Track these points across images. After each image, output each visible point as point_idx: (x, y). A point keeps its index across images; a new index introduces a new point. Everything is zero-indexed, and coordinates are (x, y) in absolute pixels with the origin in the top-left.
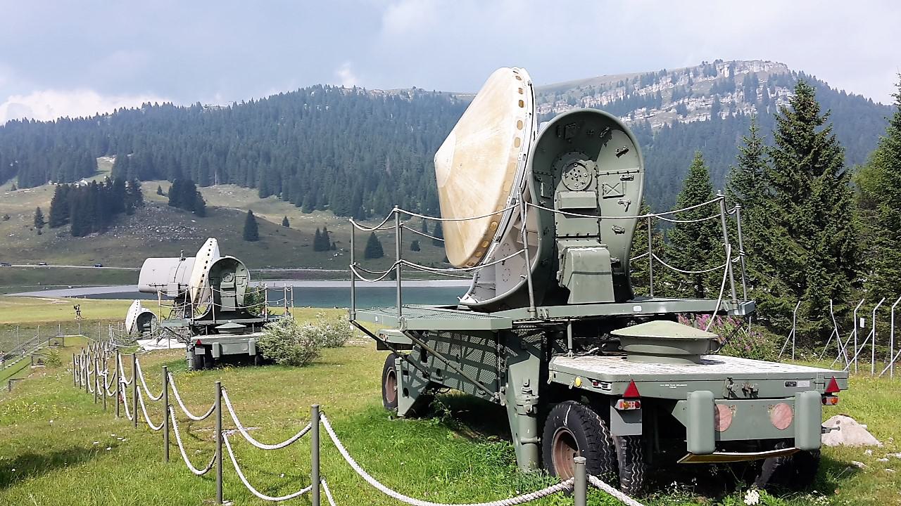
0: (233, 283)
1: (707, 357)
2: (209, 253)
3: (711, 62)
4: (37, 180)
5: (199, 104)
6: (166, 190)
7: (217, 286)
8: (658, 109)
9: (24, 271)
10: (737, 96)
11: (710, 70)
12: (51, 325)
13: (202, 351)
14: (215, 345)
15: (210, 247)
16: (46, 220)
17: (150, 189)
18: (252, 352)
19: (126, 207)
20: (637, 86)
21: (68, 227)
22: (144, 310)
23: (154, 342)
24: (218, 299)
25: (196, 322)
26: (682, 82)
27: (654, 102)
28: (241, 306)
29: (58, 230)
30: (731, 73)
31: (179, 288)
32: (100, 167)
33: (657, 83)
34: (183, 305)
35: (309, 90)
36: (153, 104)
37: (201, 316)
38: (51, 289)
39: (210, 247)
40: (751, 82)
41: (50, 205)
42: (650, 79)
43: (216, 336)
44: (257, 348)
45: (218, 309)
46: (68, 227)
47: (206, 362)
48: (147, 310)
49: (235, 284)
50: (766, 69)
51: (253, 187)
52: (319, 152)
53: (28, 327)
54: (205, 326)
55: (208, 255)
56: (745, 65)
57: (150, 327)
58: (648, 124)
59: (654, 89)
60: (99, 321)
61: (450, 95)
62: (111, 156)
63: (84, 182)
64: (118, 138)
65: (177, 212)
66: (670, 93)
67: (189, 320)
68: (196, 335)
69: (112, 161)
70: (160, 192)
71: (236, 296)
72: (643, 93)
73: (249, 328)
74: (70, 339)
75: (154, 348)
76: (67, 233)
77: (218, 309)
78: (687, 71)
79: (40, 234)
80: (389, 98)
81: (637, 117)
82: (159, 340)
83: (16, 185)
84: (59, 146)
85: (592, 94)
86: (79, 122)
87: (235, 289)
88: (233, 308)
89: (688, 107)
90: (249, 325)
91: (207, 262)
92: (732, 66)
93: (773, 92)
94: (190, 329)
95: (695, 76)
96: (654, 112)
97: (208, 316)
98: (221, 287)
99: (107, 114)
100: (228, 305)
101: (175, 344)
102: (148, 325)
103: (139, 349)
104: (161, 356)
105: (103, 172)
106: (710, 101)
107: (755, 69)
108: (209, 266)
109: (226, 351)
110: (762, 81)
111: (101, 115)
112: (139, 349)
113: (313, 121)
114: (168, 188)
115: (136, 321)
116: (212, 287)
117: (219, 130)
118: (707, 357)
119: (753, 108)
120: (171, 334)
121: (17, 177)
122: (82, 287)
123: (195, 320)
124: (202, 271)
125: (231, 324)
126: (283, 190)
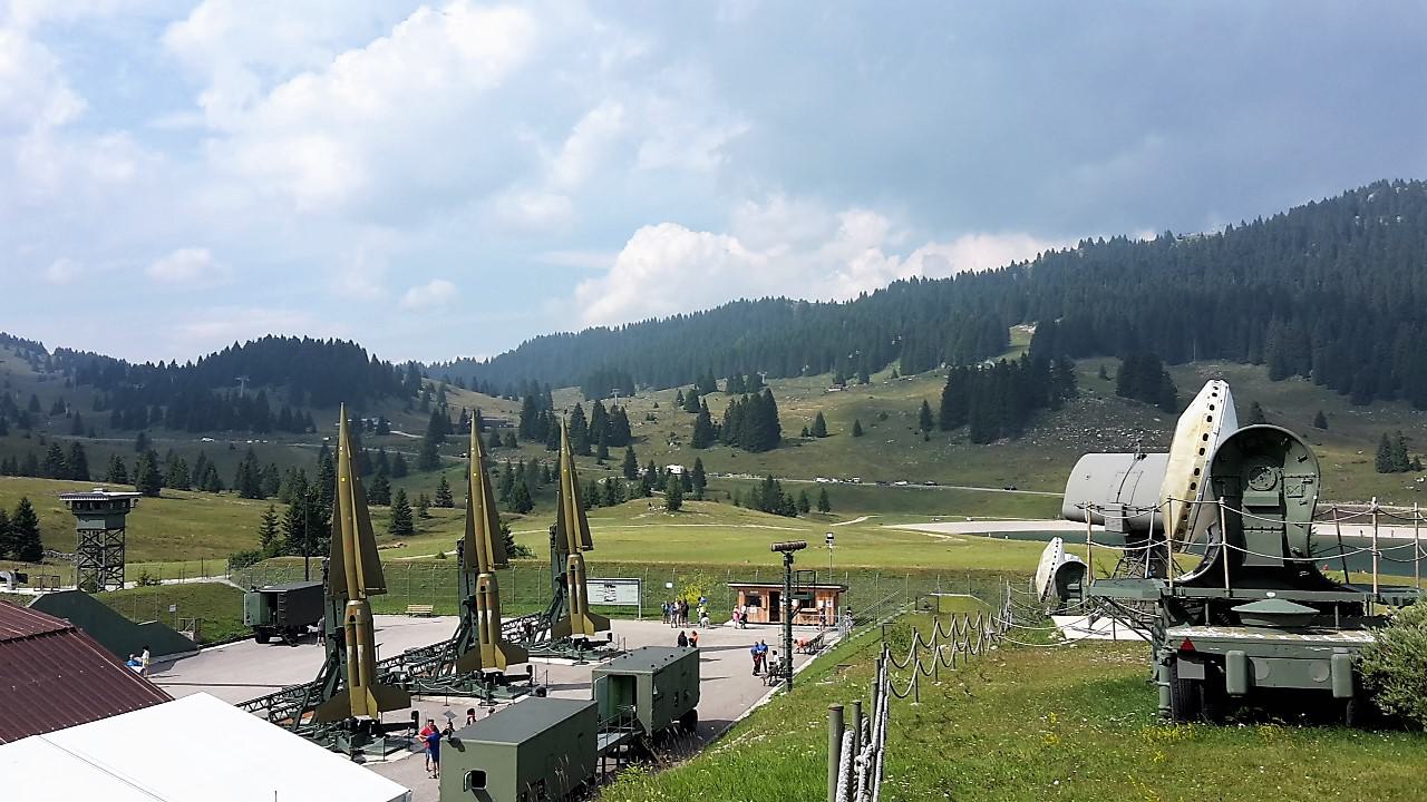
0: (1275, 494)
2: (1207, 418)
4: (921, 364)
5: (1169, 233)
6: (1112, 373)
7: (1235, 499)
9: (871, 490)
12: (926, 575)
13: (1193, 671)
14: (1233, 656)
15: (1213, 401)
16: (936, 419)
17: (1087, 369)
18: (1340, 688)
19: (1051, 399)
21: (967, 430)
22: (1068, 558)
23: (1083, 621)
24: (1236, 533)
25: (1179, 590)
28: (1300, 555)
29: (953, 433)
31: (1124, 514)
32: (1015, 341)
34: (1146, 544)
35: (1364, 192)
36: (1095, 241)
37: (1189, 576)
38: (942, 520)
39: (1213, 401)
41: (941, 397)
43: (1235, 633)
44: (1356, 678)
45: (1236, 558)
46: (967, 430)
47: (1206, 700)
48: (1076, 559)
49: (1281, 497)
51: (1258, 362)
52: (1384, 298)
53: (894, 576)
54: (1202, 602)
55: (1210, 419)
57: (1080, 591)
60: (1000, 573)
62: (1030, 325)
63: (990, 362)
64: (1042, 295)
65: (1130, 404)
67: (1159, 584)
68: (1179, 623)
69: (1032, 330)
70: (1103, 375)
71: (1284, 529)
73: (1325, 617)
74: (953, 601)
75: (1081, 635)
76: (963, 438)
77: (1236, 558)
79: (927, 439)
82: (1093, 620)
83: (898, 370)
84: (958, 311)
86: (988, 275)
87: (1281, 509)
88: (1275, 558)
90: (1326, 608)
91: (1205, 437)
94: (1161, 605)
97: (1211, 577)
98: (1244, 503)
99: (1027, 261)
100: (1263, 550)
101: (1125, 633)
103: (1054, 635)
104: (1096, 658)
105: (1015, 348)
108: (1211, 448)
109: (1265, 676)
111: (1018, 263)
112: (1054, 635)
113: (1372, 243)
114: (1116, 368)
115: (1053, 576)
116: (1221, 501)
117: (1201, 272)
120: (1117, 611)
121: (899, 360)
122: (986, 520)
123: (1176, 584)
124: (1193, 461)
125: (1273, 601)
126: (1314, 364)
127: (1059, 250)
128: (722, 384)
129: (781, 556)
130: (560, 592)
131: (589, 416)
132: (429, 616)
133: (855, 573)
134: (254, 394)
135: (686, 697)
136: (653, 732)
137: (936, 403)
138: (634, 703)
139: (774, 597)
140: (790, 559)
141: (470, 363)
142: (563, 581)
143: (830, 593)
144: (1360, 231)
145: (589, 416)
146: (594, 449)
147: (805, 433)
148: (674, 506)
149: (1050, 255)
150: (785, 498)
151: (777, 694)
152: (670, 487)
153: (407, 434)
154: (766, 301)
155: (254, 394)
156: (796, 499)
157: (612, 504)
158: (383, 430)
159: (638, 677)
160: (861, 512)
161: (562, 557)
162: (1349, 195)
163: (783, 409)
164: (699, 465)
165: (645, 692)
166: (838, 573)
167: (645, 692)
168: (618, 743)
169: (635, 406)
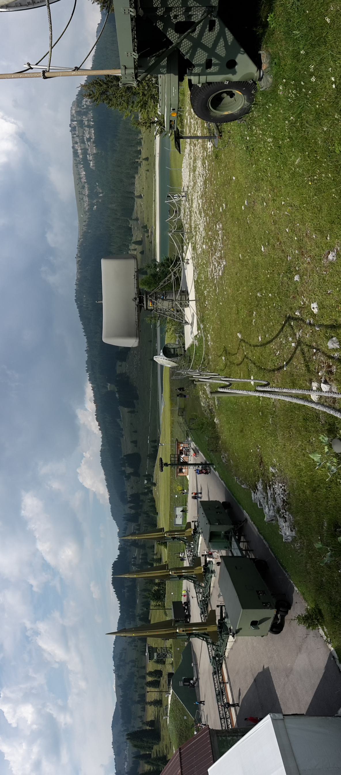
1: (95, 48)
3: (70, 128)
5: (86, 351)
8: (88, 150)
10: (85, 119)
11: (73, 129)
20: (78, 159)
21: (135, 401)
22: (161, 354)
26: (77, 140)
27: (85, 152)
30: (75, 121)
33: (77, 150)
40: (79, 113)
42: (75, 153)
50: (74, 108)
56: (72, 116)
57: (174, 349)
58: (94, 154)
59: (79, 151)
61: (79, 241)
66: (82, 145)
69: (109, 384)
70: (121, 366)
72: (81, 156)
78: (73, 137)
80: (80, 269)
81: (91, 159)
82: (187, 323)
85: (80, 178)
89: (88, 137)
92: (72, 120)
93: (84, 106)
95: (75, 134)
96: (89, 152)
102: (172, 351)
106: (86, 129)
107: (74, 112)
110: (78, 109)
118: (95, 48)
119: (90, 112)
127: (88, 378)
128: (123, 468)
129: (164, 468)
130: (177, 539)
131: (132, 505)
133: (172, 436)
134: (127, 589)
135: (218, 508)
137: (126, 410)
140: (166, 465)
142: (174, 538)
144: (87, 305)
145: (132, 505)
146: (141, 504)
147: (136, 446)
148: (155, 484)
149: (90, 380)
150: (133, 511)
151: (214, 469)
152: (150, 485)
154: (101, 456)
155: (127, 589)
156: (153, 449)
157: (154, 501)
158: (135, 558)
162: (78, 308)
163: (130, 452)
165: (217, 528)
166: (172, 441)
167: (217, 528)
168: (235, 538)
169: (129, 492)
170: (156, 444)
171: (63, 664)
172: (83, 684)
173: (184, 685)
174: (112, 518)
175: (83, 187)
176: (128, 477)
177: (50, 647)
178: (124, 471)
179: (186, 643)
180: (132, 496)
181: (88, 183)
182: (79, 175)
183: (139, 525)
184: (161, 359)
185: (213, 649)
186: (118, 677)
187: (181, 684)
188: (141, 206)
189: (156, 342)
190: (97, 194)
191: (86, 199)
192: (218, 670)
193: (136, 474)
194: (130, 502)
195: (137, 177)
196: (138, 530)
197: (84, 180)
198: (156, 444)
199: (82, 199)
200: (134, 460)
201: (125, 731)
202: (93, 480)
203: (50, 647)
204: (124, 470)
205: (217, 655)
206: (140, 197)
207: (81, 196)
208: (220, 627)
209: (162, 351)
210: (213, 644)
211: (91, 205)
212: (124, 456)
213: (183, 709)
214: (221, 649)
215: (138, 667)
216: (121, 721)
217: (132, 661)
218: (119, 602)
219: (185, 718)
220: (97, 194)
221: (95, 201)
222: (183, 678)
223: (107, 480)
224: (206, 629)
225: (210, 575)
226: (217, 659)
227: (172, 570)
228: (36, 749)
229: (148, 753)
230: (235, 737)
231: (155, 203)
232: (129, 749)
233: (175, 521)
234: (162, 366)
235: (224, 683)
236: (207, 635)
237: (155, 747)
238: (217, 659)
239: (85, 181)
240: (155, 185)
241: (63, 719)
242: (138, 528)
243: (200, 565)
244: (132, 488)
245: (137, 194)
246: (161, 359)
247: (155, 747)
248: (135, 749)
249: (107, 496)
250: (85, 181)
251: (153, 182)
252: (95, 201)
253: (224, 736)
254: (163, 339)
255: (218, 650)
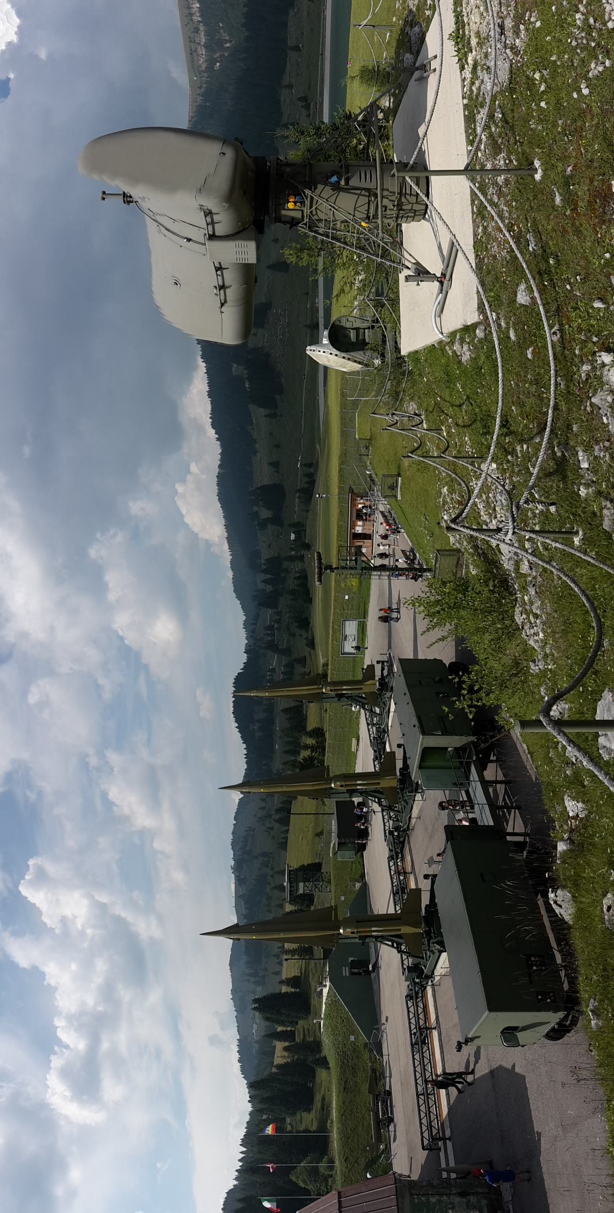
21: (277, 397)
22: (325, 341)
46: (277, 397)
70: (255, 334)
85: (191, 15)
115: (343, 355)
127: (201, 353)
128: (255, 509)
130: (348, 698)
132: (358, 741)
136: (474, 736)
137: (262, 411)
138: (447, 748)
139: (357, 536)
141: (246, 624)
143: (353, 500)
146: (283, 575)
147: (277, 472)
150: (269, 588)
153: (275, 661)
154: (218, 485)
156: (307, 480)
158: (273, 670)
159: (425, 745)
160: (315, 447)
161: (324, 696)
163: (266, 482)
164: (291, 525)
165: (436, 741)
167: (436, 741)
169: (266, 554)
170: (312, 470)
171: (145, 835)
172: (178, 876)
173: (352, 974)
174: (234, 595)
175: (197, 30)
176: (263, 524)
177: (127, 798)
178: (256, 514)
179: (358, 885)
180: (268, 561)
181: (206, 21)
182: (190, 8)
183: (279, 613)
184: (324, 354)
185: (390, 817)
186: (240, 881)
187: (346, 971)
188: (298, 65)
189: (316, 295)
190: (220, 43)
191: (202, 51)
192: (397, 853)
193: (277, 520)
194: (265, 572)
195: (291, 14)
196: (278, 621)
197: (197, 18)
198: (312, 470)
199: (196, 50)
200: (273, 495)
201: (251, 975)
202: (202, 518)
203: (127, 798)
204: (257, 512)
205: (397, 828)
206: (297, 49)
207: (193, 46)
208: (401, 781)
209: (326, 333)
210: (390, 808)
211: (211, 62)
212: (257, 488)
213: (349, 1020)
214: (402, 817)
215: (272, 869)
216: (245, 958)
217: (264, 854)
218: (244, 746)
219: (352, 1038)
220: (220, 43)
221: (218, 55)
222: (351, 959)
223: (225, 517)
224: (379, 783)
225: (388, 694)
226: (396, 834)
227: (337, 778)
228: (101, 965)
229: (289, 1029)
230: (445, 1198)
231: (322, 60)
232: (258, 1026)
233: (343, 647)
234: (326, 368)
235: (405, 873)
236: (381, 793)
237: (301, 1022)
238: (396, 834)
239: (200, 19)
240: (324, 26)
241: (146, 928)
242: (277, 618)
243: (374, 678)
244: (270, 546)
245: (291, 43)
246: (324, 354)
247: (301, 1022)
248: (267, 1023)
249: (227, 556)
250: (200, 19)
251: (320, 22)
252: (218, 55)
253: (424, 1195)
254: (328, 311)
255: (398, 820)
